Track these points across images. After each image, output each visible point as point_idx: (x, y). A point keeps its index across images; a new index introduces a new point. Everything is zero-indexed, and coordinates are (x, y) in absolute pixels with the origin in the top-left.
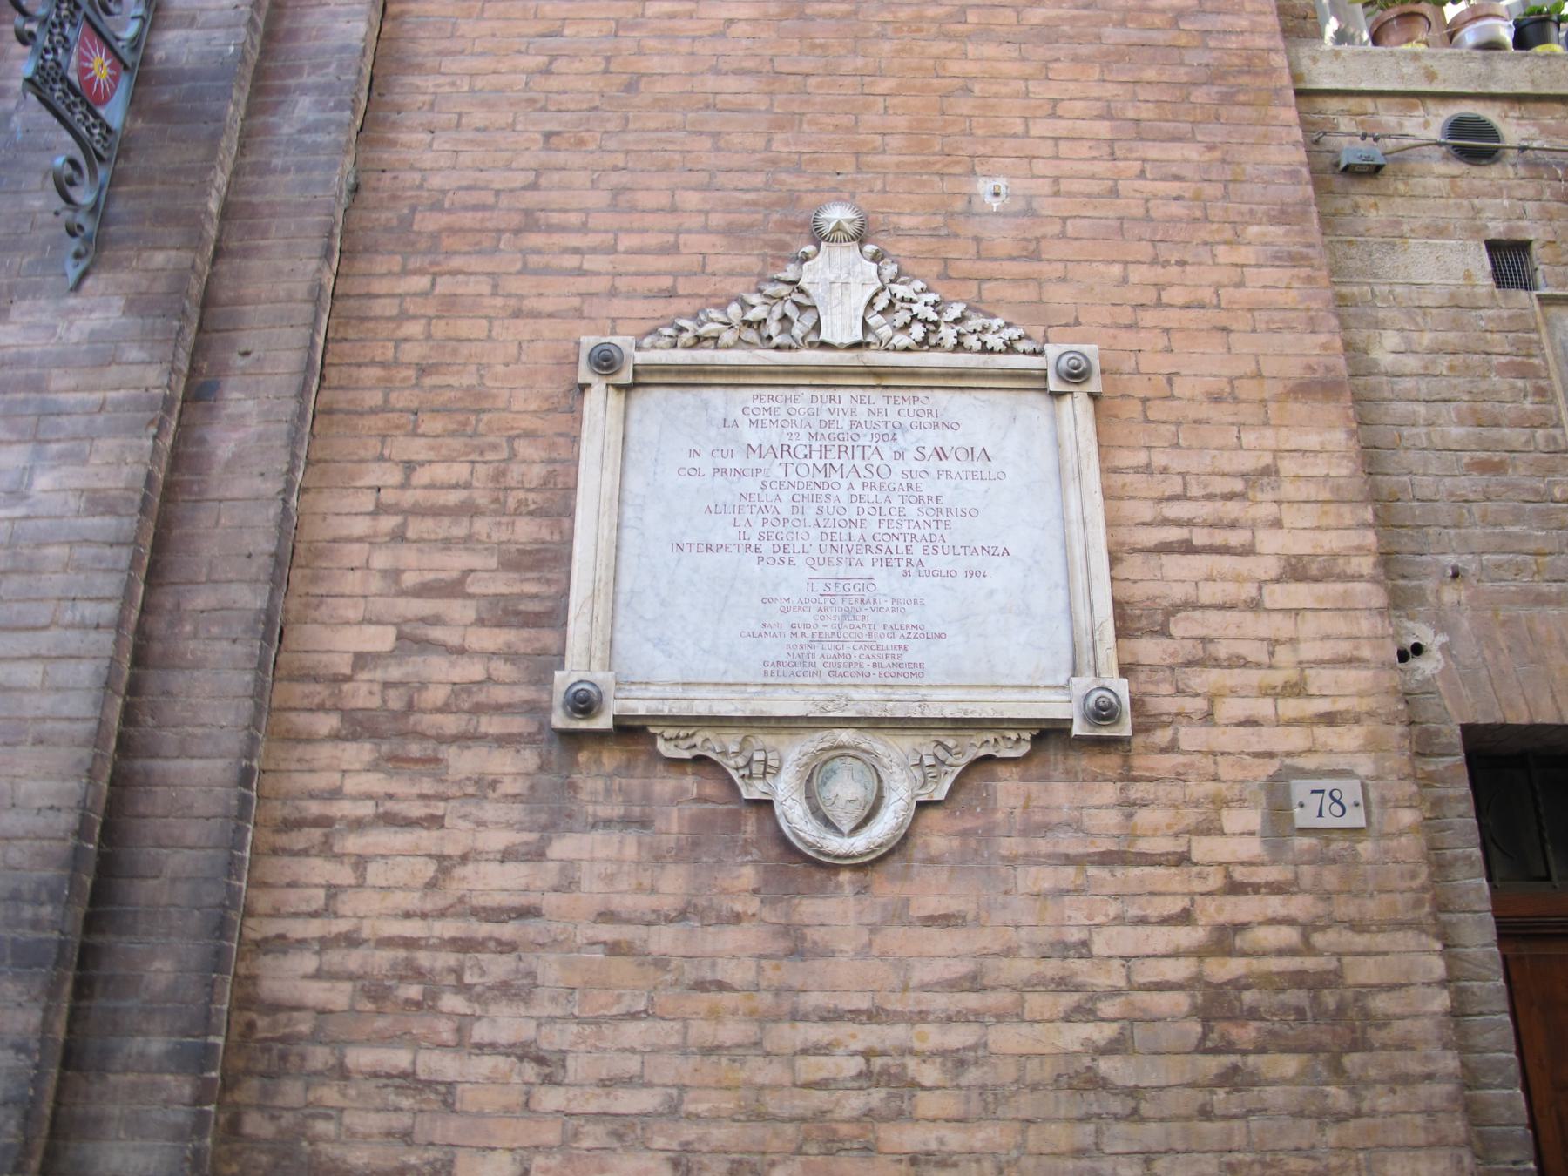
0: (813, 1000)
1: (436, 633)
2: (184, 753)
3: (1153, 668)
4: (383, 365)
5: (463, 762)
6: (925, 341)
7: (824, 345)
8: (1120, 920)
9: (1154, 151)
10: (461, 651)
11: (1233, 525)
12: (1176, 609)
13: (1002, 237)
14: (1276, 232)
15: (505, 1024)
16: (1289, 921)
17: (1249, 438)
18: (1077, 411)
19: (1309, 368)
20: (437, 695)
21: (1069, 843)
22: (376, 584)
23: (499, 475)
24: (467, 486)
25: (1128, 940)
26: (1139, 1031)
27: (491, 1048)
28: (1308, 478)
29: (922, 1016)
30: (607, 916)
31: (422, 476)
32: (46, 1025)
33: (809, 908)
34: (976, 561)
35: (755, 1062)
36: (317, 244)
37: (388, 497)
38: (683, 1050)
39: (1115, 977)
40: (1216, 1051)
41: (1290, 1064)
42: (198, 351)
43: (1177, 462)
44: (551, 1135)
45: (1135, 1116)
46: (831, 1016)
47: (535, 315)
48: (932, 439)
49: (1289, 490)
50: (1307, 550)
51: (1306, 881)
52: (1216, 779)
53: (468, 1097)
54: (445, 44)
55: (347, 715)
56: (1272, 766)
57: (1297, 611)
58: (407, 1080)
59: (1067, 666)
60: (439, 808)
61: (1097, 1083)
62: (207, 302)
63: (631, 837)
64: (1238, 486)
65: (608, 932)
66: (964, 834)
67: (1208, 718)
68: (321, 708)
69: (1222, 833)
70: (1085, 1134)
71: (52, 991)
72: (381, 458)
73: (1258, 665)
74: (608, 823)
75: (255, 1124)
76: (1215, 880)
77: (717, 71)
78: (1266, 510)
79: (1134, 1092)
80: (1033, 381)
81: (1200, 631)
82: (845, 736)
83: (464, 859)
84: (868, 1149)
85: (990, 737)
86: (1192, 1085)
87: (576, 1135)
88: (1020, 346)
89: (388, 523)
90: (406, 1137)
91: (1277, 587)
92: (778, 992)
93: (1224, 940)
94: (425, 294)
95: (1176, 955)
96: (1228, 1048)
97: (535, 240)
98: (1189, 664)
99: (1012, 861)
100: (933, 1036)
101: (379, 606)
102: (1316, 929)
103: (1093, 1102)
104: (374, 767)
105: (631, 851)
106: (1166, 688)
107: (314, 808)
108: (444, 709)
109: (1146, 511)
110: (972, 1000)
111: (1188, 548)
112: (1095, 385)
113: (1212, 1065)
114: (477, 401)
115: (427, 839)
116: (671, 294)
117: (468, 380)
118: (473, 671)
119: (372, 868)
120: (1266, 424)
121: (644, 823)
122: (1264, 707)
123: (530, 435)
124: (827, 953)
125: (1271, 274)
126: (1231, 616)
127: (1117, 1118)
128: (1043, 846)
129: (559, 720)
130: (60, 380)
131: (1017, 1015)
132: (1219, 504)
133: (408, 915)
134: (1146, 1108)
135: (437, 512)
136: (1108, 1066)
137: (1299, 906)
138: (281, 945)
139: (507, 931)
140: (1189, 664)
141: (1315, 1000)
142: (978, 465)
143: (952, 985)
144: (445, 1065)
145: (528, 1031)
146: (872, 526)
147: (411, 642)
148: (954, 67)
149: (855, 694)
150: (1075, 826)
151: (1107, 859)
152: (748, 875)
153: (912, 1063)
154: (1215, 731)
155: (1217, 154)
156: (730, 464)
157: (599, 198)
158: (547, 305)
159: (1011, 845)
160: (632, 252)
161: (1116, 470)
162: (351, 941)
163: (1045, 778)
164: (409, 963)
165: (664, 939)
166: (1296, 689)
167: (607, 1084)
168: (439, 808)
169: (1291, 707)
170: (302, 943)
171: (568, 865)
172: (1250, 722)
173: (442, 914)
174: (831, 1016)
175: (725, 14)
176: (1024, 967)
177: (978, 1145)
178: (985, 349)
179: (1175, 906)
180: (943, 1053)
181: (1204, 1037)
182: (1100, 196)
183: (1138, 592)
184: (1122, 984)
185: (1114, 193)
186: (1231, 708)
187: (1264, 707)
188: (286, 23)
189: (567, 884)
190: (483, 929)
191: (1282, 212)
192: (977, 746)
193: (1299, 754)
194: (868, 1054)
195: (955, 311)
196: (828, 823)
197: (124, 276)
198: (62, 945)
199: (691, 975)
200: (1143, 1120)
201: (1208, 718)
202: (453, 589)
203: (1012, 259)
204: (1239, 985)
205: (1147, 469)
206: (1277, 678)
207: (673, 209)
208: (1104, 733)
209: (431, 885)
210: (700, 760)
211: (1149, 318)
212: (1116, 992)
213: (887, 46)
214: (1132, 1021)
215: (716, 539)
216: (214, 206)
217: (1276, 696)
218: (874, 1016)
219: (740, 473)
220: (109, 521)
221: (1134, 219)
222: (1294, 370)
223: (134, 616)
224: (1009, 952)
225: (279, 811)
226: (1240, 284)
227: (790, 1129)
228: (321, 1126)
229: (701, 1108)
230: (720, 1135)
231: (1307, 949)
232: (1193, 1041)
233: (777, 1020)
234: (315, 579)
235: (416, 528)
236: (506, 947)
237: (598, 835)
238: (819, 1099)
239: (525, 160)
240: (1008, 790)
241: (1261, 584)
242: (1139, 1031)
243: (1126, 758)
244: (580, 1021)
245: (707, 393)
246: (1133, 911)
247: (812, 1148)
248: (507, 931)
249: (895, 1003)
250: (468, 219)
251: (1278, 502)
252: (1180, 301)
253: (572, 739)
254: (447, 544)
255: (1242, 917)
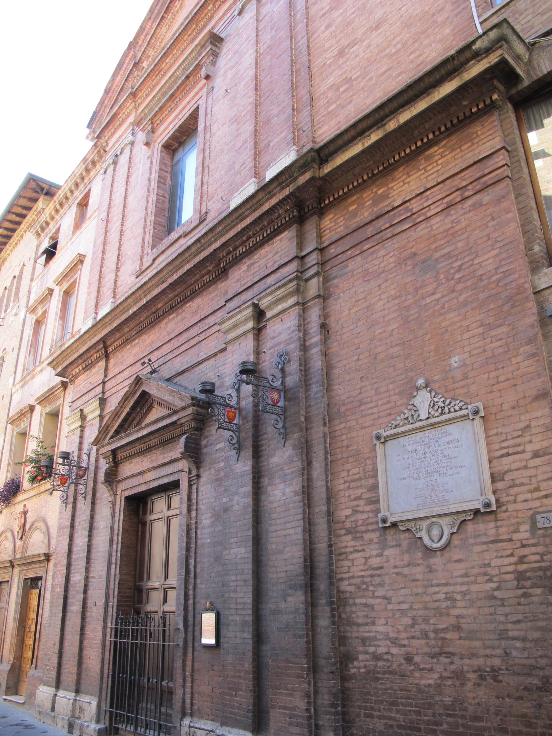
0: (435, 582)
1: (359, 509)
2: (319, 543)
3: (501, 490)
4: (340, 448)
5: (367, 536)
6: (442, 413)
7: (421, 420)
8: (497, 557)
9: (494, 333)
10: (363, 512)
11: (519, 445)
12: (506, 472)
13: (458, 375)
14: (527, 348)
15: (380, 592)
16: (537, 553)
17: (523, 418)
18: (478, 421)
19: (539, 390)
20: (360, 522)
21: (484, 539)
22: (347, 500)
23: (364, 469)
24: (359, 473)
25: (499, 562)
26: (503, 584)
27: (378, 597)
28: (538, 426)
29: (456, 584)
30: (395, 567)
31: (351, 473)
32: (306, 599)
33: (432, 561)
34: (458, 470)
35: (425, 596)
36: (321, 423)
37: (346, 479)
38: (412, 595)
39: (495, 572)
40: (521, 588)
41: (539, 591)
42: (308, 453)
43: (504, 430)
44: (390, 615)
45: (503, 605)
46: (438, 585)
47: (365, 427)
48: (446, 439)
49: (534, 431)
50: (539, 448)
51: (541, 542)
52: (518, 518)
53: (376, 607)
54: (339, 359)
55: (346, 529)
56: (531, 512)
57: (536, 467)
58: (366, 605)
59: (480, 494)
60: (364, 547)
61: (494, 598)
62: (307, 442)
63: (398, 548)
64: (520, 433)
65: (396, 570)
66: (461, 539)
67: (515, 501)
68: (342, 529)
69: (520, 532)
70: (492, 610)
71: (306, 592)
72: (343, 470)
73: (527, 484)
74: (393, 546)
75: (343, 616)
76: (519, 545)
77: (392, 347)
78: (528, 438)
79: (503, 599)
80: (465, 417)
81: (512, 478)
82: (434, 520)
83: (369, 558)
84: (448, 615)
85: (464, 515)
86: (516, 597)
87: (395, 614)
88: (463, 407)
89: (347, 485)
90: (367, 616)
91: (531, 461)
92: (428, 580)
93: (522, 560)
94: (344, 428)
95: (510, 565)
96: (523, 587)
97: (362, 408)
98: (510, 487)
99: (472, 545)
100: (459, 588)
101: (348, 504)
102: (545, 555)
103: (493, 602)
104: (352, 540)
105: (398, 552)
106: (504, 495)
107: (344, 550)
108: (362, 525)
109: (497, 446)
110: (466, 579)
111: (508, 454)
112: (482, 413)
113: (520, 592)
114: (358, 452)
115: (362, 554)
116: (390, 414)
117: (356, 447)
118: (365, 516)
119: (355, 562)
120: (527, 412)
121: (400, 545)
122: (529, 496)
123: (368, 458)
124: (437, 571)
125: (527, 363)
126: (519, 472)
127: (499, 606)
128: (479, 540)
129: (381, 525)
130: (286, 468)
131: (475, 582)
132: (515, 440)
133: (362, 571)
134: (505, 603)
135: (355, 481)
136: (496, 593)
137: (540, 549)
138: (342, 579)
139: (378, 572)
140: (510, 487)
141: (545, 574)
142: (457, 444)
143: (462, 576)
144: (371, 601)
145: (384, 593)
146: (436, 466)
147: (355, 512)
148: (443, 324)
149: (435, 509)
150: (485, 534)
151: (493, 542)
152: (420, 555)
153: (455, 595)
154: (517, 505)
155: (511, 327)
156: (407, 456)
157: (373, 392)
158: (367, 424)
159: (472, 541)
160: (381, 405)
161: (489, 436)
162: (353, 577)
163: (478, 523)
164: (363, 581)
165: (406, 571)
166: (537, 489)
167: (399, 603)
168: (364, 547)
169: (536, 495)
170: (345, 578)
171: (387, 556)
172: (526, 501)
173: (367, 570)
174: (438, 585)
175: (392, 328)
176: (476, 571)
177: (470, 613)
178: (455, 411)
179: (509, 552)
180: (461, 592)
181: (518, 585)
182: (481, 353)
183: (496, 470)
184: (498, 573)
185: (484, 351)
186: (521, 498)
187: (529, 496)
188: (308, 366)
189: (387, 561)
190: (375, 572)
191: (530, 340)
192: (462, 518)
193: (538, 507)
194: (446, 593)
195: (448, 402)
196: (433, 541)
197: (291, 441)
198: (306, 584)
199: (411, 579)
200: (505, 606)
201: (515, 501)
202: (359, 498)
203: (461, 381)
204: (526, 571)
205: (497, 434)
206: (532, 487)
207: (388, 391)
208: (488, 510)
209: (365, 564)
210: (408, 529)
211: (495, 388)
212: (497, 575)
213: (427, 324)
214: (501, 582)
215: (405, 476)
216: (302, 419)
217: (532, 492)
218: (446, 584)
219: (408, 458)
220: (298, 497)
221: (490, 358)
222: (534, 393)
223: (307, 516)
224: (473, 567)
225: (338, 552)
226: (519, 369)
227: (433, 611)
228: (354, 615)
229: (416, 607)
230: (420, 613)
231: (542, 560)
232: (515, 586)
233: (428, 587)
234: (336, 501)
235: (353, 485)
236: (379, 576)
237: (392, 549)
238: (437, 604)
239: (358, 386)
240: (470, 527)
241: (527, 461)
242: (503, 584)
243: (496, 515)
244: (393, 590)
245: (399, 439)
246: (500, 555)
247: (437, 615)
248: (378, 572)
249: (451, 581)
250: (349, 406)
251: (531, 435)
252: (503, 380)
253: (385, 528)
254: (357, 488)
255: (525, 554)
